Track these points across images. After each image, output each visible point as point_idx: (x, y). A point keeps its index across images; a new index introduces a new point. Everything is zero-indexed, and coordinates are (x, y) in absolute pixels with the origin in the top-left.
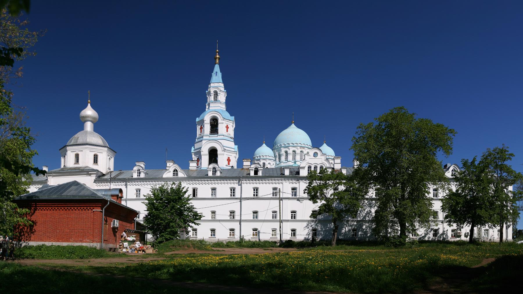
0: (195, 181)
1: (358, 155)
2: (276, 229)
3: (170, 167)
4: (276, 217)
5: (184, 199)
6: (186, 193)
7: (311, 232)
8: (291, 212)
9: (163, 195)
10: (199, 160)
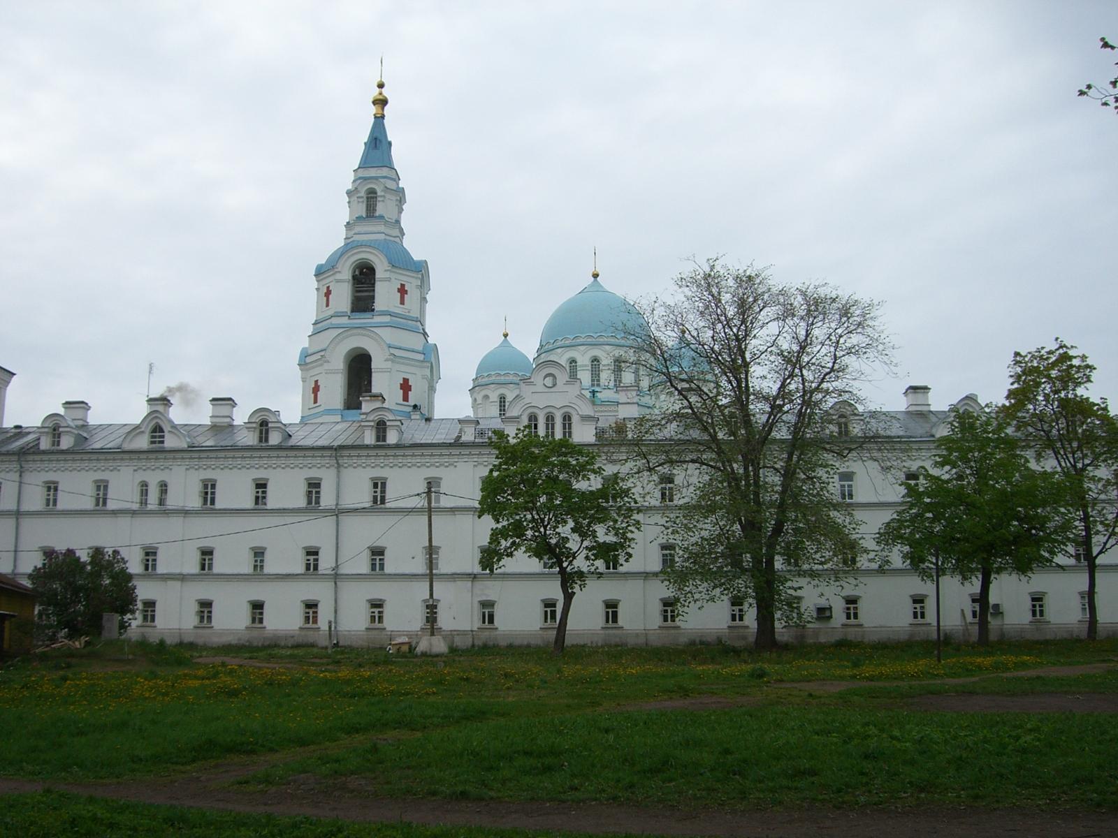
2: (926, 596)
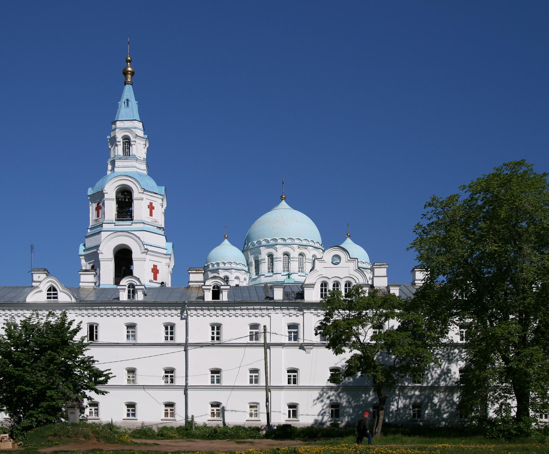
0: (93, 309)
1: (428, 258)
2: (258, 404)
3: (40, 282)
4: (256, 381)
5: (73, 344)
6: (78, 334)
7: (329, 410)
8: (288, 372)
9: (29, 336)
10: (95, 268)
